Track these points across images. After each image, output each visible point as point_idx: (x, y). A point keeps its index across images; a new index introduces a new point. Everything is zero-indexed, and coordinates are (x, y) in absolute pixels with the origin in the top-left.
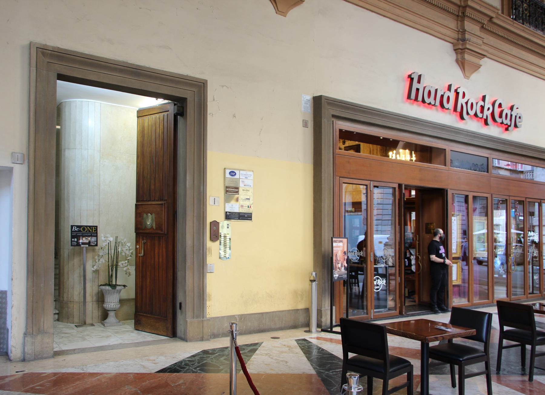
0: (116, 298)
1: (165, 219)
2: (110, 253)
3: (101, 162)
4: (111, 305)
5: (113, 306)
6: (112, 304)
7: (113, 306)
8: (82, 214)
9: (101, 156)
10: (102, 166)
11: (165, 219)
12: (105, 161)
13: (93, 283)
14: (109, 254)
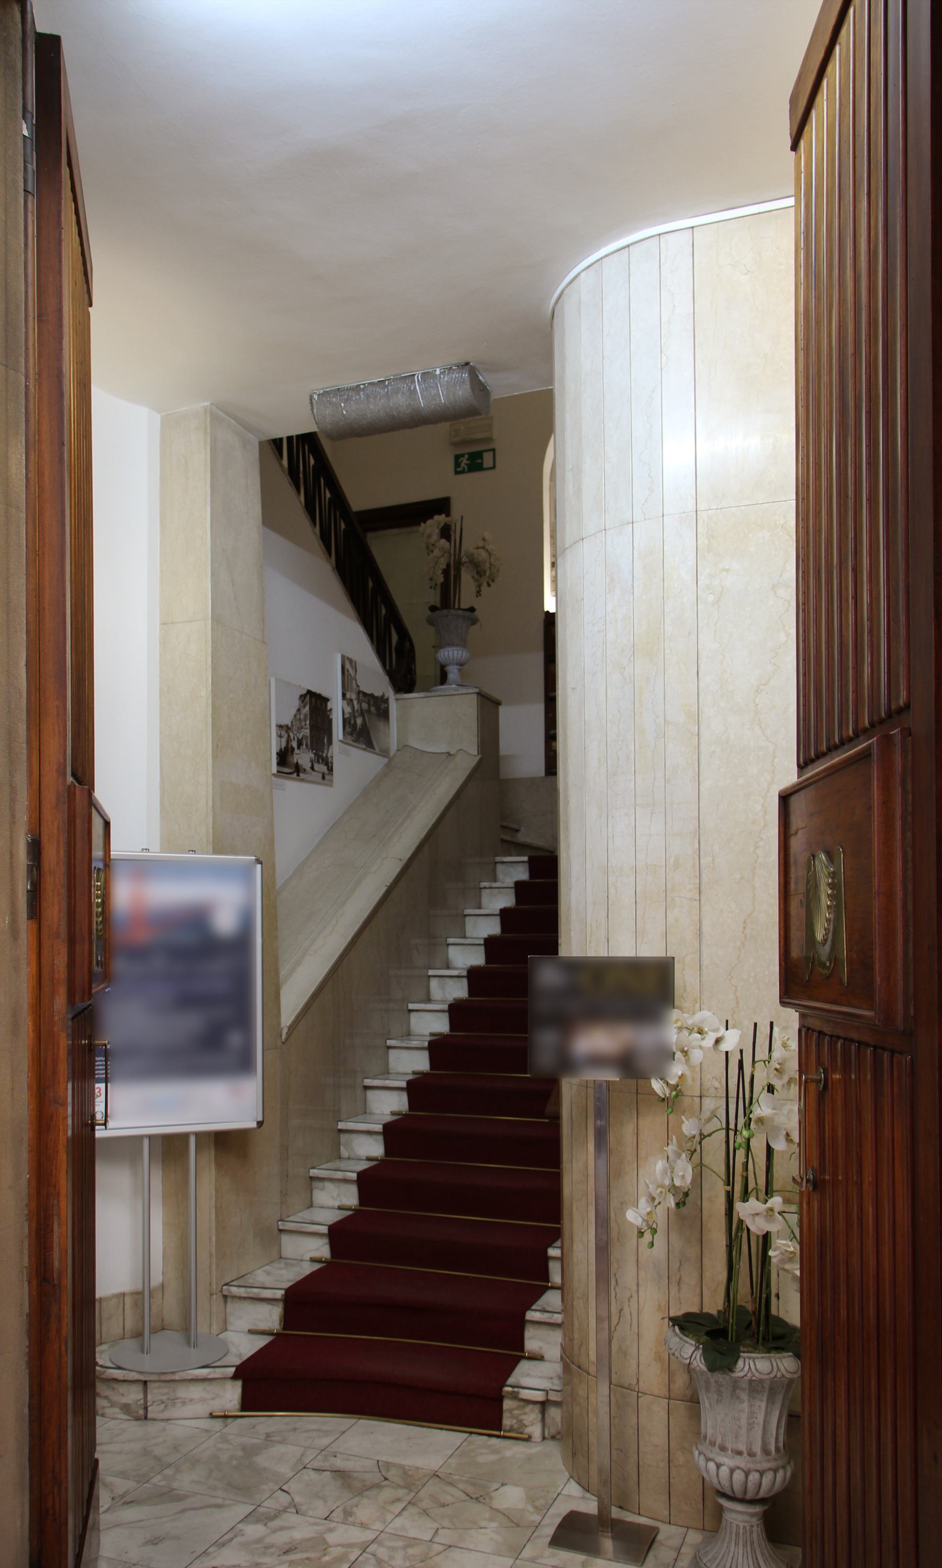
0: (750, 1426)
1: (889, 895)
2: (732, 1126)
3: (702, 579)
4: (718, 1466)
5: (732, 1471)
6: (728, 1461)
7: (747, 1474)
8: (612, 891)
9: (703, 541)
10: (711, 598)
11: (889, 895)
12: (727, 571)
13: (674, 1291)
14: (728, 1129)
